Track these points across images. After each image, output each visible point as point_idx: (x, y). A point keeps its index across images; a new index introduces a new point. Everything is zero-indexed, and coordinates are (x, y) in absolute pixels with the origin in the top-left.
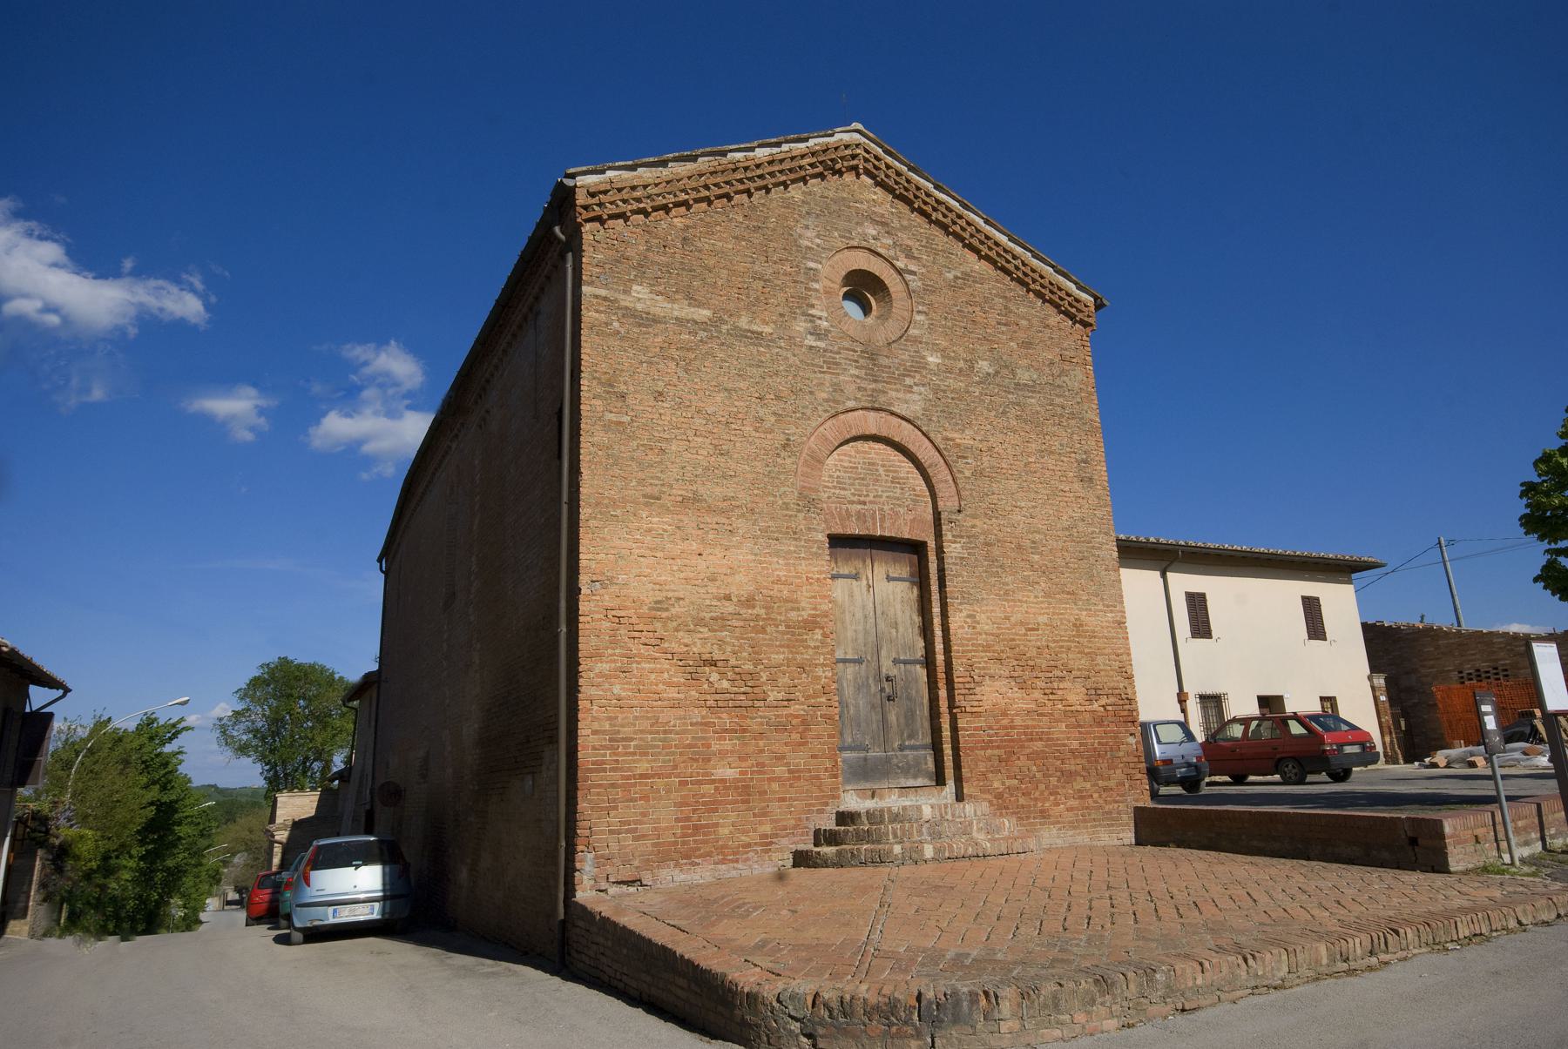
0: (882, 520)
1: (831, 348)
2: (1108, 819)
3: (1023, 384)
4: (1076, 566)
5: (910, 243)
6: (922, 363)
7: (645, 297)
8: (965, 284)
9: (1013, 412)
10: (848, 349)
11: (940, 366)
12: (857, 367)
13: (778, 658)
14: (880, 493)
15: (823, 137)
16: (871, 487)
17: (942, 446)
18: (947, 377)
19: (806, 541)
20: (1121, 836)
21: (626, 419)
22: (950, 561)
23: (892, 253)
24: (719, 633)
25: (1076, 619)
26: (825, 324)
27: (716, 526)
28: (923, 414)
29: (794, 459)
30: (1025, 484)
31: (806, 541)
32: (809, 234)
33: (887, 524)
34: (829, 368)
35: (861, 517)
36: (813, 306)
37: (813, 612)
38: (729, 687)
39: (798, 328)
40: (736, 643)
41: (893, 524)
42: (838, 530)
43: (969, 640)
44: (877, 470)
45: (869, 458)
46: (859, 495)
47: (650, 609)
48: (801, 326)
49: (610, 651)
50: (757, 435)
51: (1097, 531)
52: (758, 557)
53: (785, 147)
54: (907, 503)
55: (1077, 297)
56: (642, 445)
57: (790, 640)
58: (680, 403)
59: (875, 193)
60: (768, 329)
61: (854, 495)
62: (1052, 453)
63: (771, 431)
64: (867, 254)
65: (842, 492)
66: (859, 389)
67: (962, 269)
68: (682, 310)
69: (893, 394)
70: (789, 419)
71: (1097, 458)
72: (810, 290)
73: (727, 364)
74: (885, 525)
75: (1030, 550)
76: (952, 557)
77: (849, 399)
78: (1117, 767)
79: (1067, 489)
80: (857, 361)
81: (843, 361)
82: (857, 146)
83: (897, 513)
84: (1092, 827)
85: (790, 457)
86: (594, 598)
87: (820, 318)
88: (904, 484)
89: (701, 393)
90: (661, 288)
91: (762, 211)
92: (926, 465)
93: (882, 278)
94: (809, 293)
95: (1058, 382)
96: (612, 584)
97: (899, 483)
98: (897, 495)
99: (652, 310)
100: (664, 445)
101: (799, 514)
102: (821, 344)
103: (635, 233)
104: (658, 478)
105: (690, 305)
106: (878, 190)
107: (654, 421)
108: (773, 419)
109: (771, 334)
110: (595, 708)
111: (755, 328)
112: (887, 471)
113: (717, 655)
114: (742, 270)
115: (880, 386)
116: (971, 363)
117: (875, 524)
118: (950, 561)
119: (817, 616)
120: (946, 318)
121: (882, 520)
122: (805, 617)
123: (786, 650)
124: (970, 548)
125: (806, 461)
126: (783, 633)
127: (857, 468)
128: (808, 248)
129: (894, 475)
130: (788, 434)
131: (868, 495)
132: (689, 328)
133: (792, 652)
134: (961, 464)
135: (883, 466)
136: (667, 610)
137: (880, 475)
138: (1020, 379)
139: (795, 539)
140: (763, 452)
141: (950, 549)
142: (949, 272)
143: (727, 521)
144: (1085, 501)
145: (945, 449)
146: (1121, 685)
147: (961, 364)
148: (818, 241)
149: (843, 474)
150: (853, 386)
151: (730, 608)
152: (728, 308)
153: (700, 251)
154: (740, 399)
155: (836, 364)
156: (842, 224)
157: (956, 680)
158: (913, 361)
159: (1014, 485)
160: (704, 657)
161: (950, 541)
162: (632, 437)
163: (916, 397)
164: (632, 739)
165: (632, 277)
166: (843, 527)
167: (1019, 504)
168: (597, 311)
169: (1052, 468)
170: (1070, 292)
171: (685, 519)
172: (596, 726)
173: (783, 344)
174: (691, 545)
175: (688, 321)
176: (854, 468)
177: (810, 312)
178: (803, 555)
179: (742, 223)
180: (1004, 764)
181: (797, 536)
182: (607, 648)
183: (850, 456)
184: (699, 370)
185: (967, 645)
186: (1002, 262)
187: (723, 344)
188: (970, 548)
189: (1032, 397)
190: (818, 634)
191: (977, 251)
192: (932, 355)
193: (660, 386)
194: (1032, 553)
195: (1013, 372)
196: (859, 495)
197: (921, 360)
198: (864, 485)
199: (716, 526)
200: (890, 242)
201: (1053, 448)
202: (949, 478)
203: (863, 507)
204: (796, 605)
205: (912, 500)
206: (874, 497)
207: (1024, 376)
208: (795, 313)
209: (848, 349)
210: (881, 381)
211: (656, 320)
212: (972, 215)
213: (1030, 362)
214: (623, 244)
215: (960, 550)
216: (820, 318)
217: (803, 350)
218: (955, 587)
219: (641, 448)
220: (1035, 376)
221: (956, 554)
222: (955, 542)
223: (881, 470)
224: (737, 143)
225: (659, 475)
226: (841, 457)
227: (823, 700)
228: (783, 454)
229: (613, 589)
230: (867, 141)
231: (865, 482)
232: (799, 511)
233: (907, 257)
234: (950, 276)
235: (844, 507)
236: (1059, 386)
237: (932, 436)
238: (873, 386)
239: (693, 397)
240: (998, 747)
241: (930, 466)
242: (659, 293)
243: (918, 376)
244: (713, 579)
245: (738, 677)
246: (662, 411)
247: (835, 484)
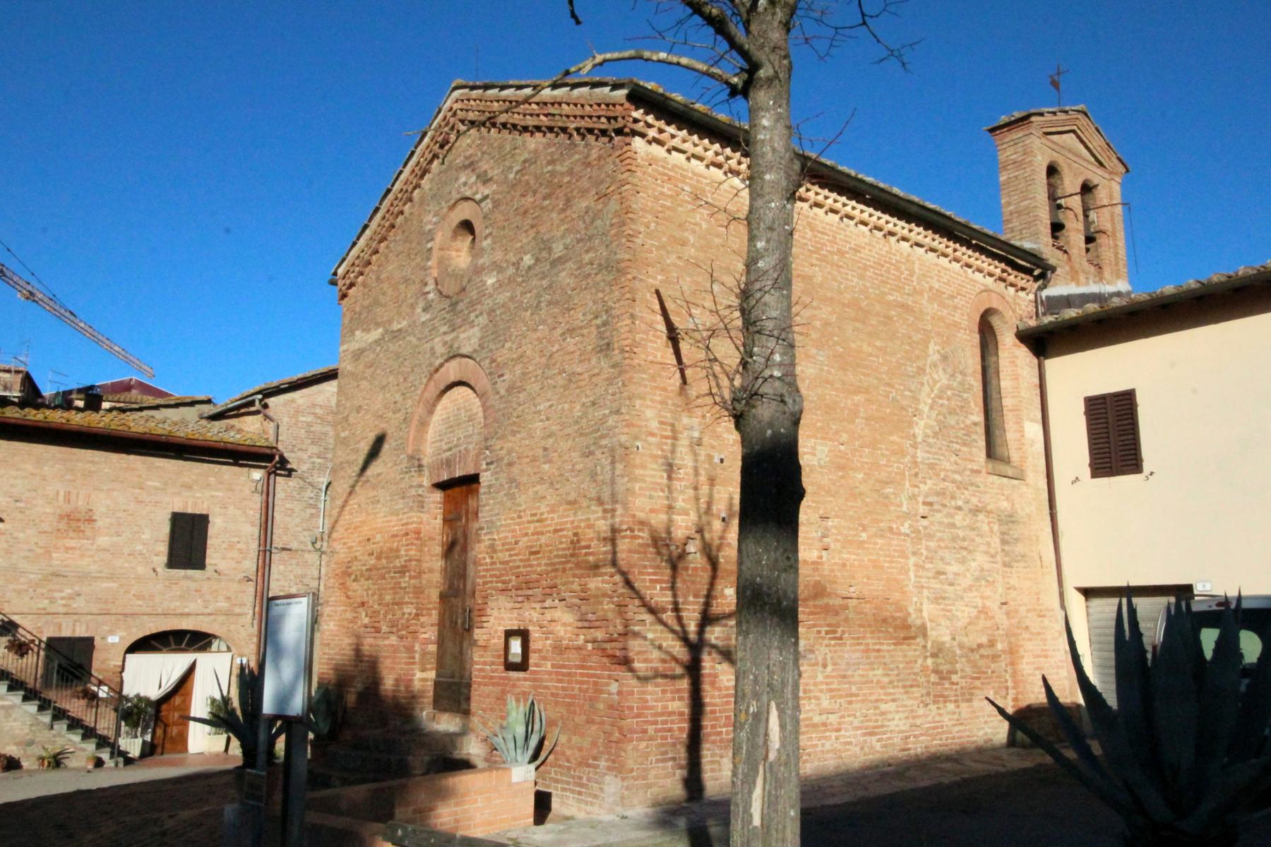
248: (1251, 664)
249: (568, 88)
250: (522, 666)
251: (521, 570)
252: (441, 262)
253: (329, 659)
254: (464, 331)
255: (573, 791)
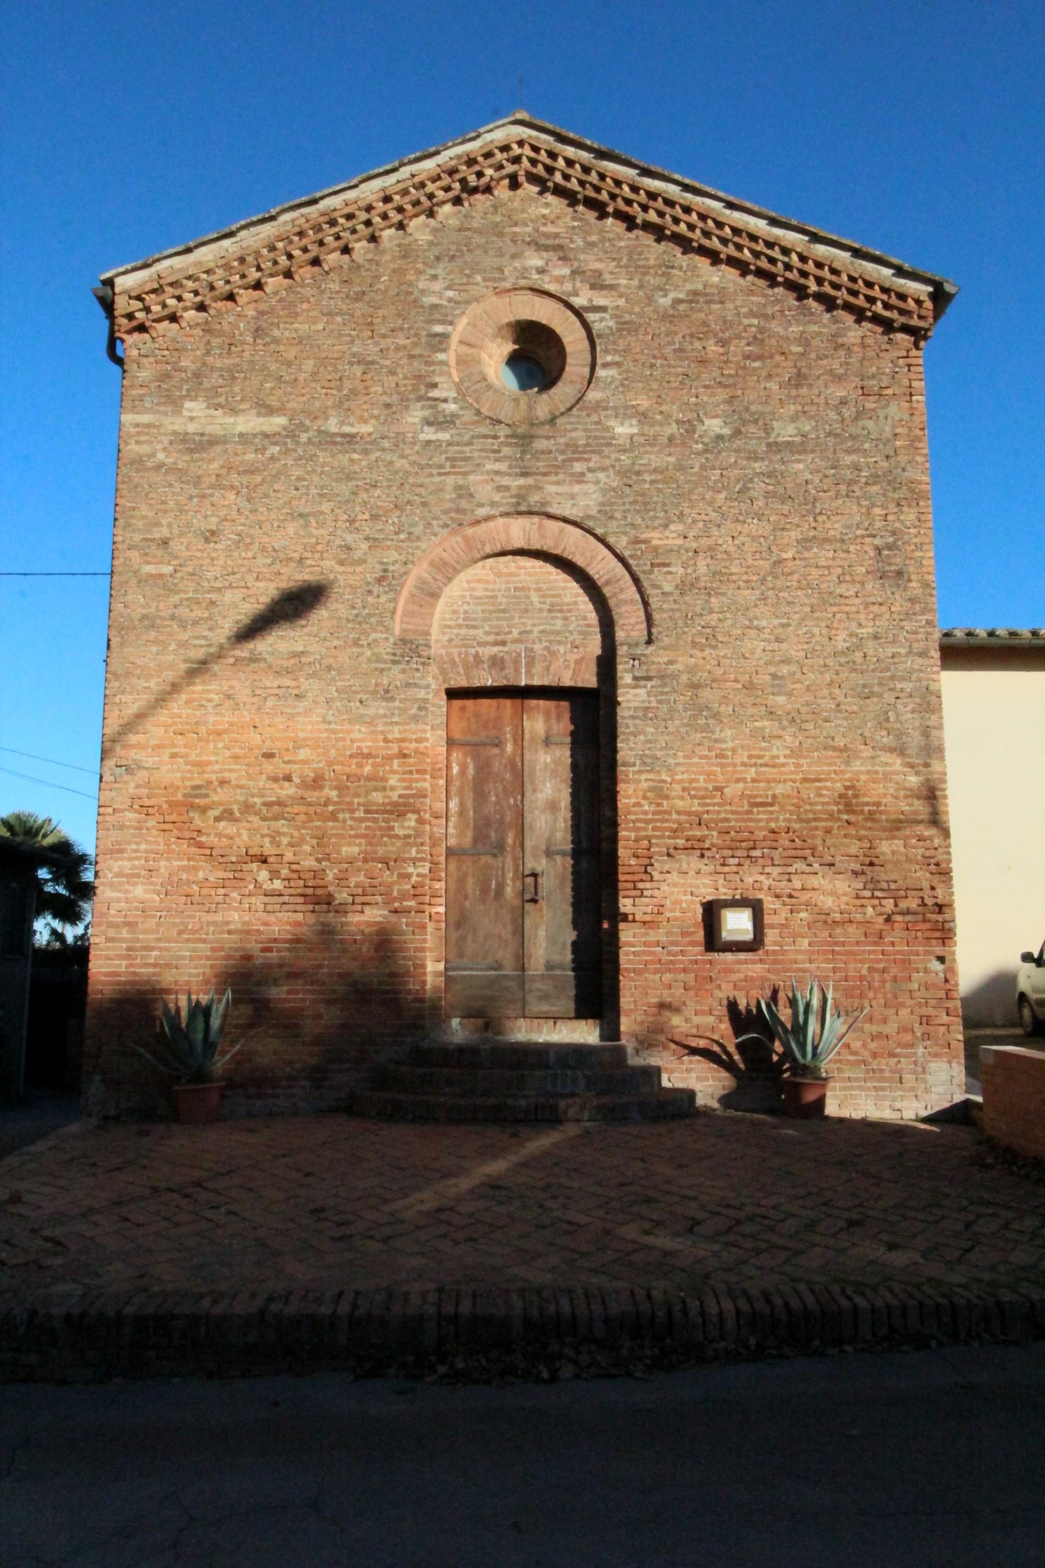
0: (530, 664)
1: (457, 439)
2: (873, 1079)
3: (784, 442)
4: (855, 708)
5: (598, 266)
6: (604, 438)
7: (199, 414)
8: (692, 309)
9: (758, 488)
10: (486, 437)
11: (635, 439)
12: (497, 460)
13: (350, 850)
14: (529, 628)
15: (462, 143)
16: (516, 621)
17: (627, 554)
18: (647, 452)
19: (401, 701)
20: (898, 1105)
21: (167, 569)
22: (626, 713)
23: (568, 287)
24: (273, 823)
25: (847, 788)
26: (452, 407)
27: (276, 691)
28: (599, 512)
29: (391, 596)
30: (770, 593)
31: (401, 701)
32: (437, 286)
33: (538, 668)
34: (453, 467)
35: (496, 663)
36: (435, 386)
37: (406, 792)
38: (281, 888)
39: (410, 420)
40: (296, 834)
41: (548, 668)
42: (461, 681)
43: (647, 822)
44: (527, 597)
45: (515, 582)
46: (497, 634)
47: (185, 795)
48: (416, 415)
49: (134, 847)
50: (342, 569)
51: (903, 651)
52: (333, 726)
53: (405, 172)
54: (571, 638)
55: (901, 290)
56: (188, 599)
57: (368, 828)
58: (239, 541)
59: (547, 205)
60: (365, 429)
61: (488, 633)
62: (826, 540)
63: (362, 561)
64: (529, 296)
65: (471, 632)
66: (499, 489)
67: (689, 287)
68: (249, 423)
69: (551, 489)
70: (389, 543)
71: (915, 540)
72: (432, 363)
73: (305, 483)
74: (534, 671)
75: (770, 690)
76: (630, 708)
77: (481, 505)
78: (902, 1005)
79: (852, 592)
80: (498, 451)
81: (476, 454)
82: (521, 143)
83: (553, 654)
84: (842, 1089)
85: (386, 593)
86: (117, 785)
87: (445, 401)
88: (569, 611)
89: (267, 527)
90: (222, 400)
91: (369, 270)
92: (599, 583)
93: (552, 326)
94: (432, 368)
95: (853, 430)
96: (139, 768)
97: (561, 611)
98: (558, 628)
99: (208, 430)
100: (213, 596)
101: (394, 667)
102: (444, 436)
103: (191, 336)
104: (204, 637)
105: (259, 414)
106: (550, 198)
107: (204, 568)
108: (364, 546)
109: (370, 434)
110: (113, 912)
111: (347, 429)
112: (543, 596)
113: (268, 849)
114: (336, 356)
115: (530, 481)
116: (690, 427)
117: (517, 671)
118: (626, 713)
119: (412, 796)
120: (652, 366)
121: (530, 664)
122: (395, 798)
123: (363, 841)
124: (662, 693)
125: (413, 596)
126: (361, 820)
127: (496, 597)
128: (435, 307)
129: (554, 600)
130: (388, 564)
131: (510, 632)
132: (256, 444)
133: (370, 844)
134: (657, 575)
135: (539, 590)
136: (206, 796)
137: (532, 603)
138: (778, 435)
139: (387, 700)
140: (348, 590)
141: (629, 697)
142: (665, 296)
143: (293, 684)
144: (884, 608)
145: (631, 556)
146: (925, 885)
147: (673, 429)
148: (450, 294)
149: (472, 607)
150: (489, 487)
151: (289, 790)
152: (312, 409)
153: (278, 344)
154: (321, 525)
155: (466, 459)
156: (489, 261)
157: (621, 877)
158: (589, 437)
159: (749, 596)
160: (251, 852)
161: (629, 686)
162: (173, 591)
163: (591, 488)
164: (152, 949)
165: (184, 393)
166: (468, 679)
167: (756, 623)
168: (138, 443)
169: (825, 564)
170: (887, 285)
171: (234, 683)
172: (111, 932)
173: (387, 445)
174: (243, 716)
175: (255, 436)
176: (491, 597)
177: (431, 395)
178: (396, 719)
179: (338, 292)
180: (692, 993)
181: (390, 695)
182: (129, 843)
183: (487, 582)
184: (266, 496)
185: (645, 829)
186: (754, 263)
187: (300, 458)
188: (662, 693)
189: (799, 461)
190: (411, 820)
191: (704, 251)
192: (622, 425)
193: (213, 523)
194: (773, 694)
195: (767, 429)
196: (497, 634)
197: (606, 434)
198: (504, 619)
199: (276, 691)
200: (566, 271)
201: (832, 533)
202: (637, 597)
203: (501, 648)
204: (381, 784)
205: (580, 633)
206: (520, 633)
207: (785, 431)
208: (408, 400)
209: (486, 437)
210: (534, 474)
211: (214, 441)
212: (709, 202)
213: (800, 408)
214: (176, 354)
215: (645, 697)
216: (445, 401)
217: (417, 448)
218: (631, 749)
219: (185, 603)
220: (808, 428)
221: (637, 704)
222: (636, 687)
223: (535, 598)
224: (329, 186)
225: (206, 633)
226: (473, 585)
227: (412, 903)
228: (376, 589)
229: (143, 774)
230: (534, 133)
231: (507, 615)
232: (394, 662)
233: (593, 287)
234: (665, 301)
235: (473, 651)
236: (853, 437)
237: (611, 540)
238: (522, 481)
239: (256, 532)
240: (684, 970)
241: (608, 583)
242: (217, 407)
243: (595, 458)
244: (269, 756)
245: (295, 876)
246: (214, 555)
247: (461, 621)
248: (41, 868)
249: (806, 238)
250: (713, 940)
251: (733, 824)
252: (462, 362)
253: (213, 949)
254: (557, 483)
255: (860, 1088)
